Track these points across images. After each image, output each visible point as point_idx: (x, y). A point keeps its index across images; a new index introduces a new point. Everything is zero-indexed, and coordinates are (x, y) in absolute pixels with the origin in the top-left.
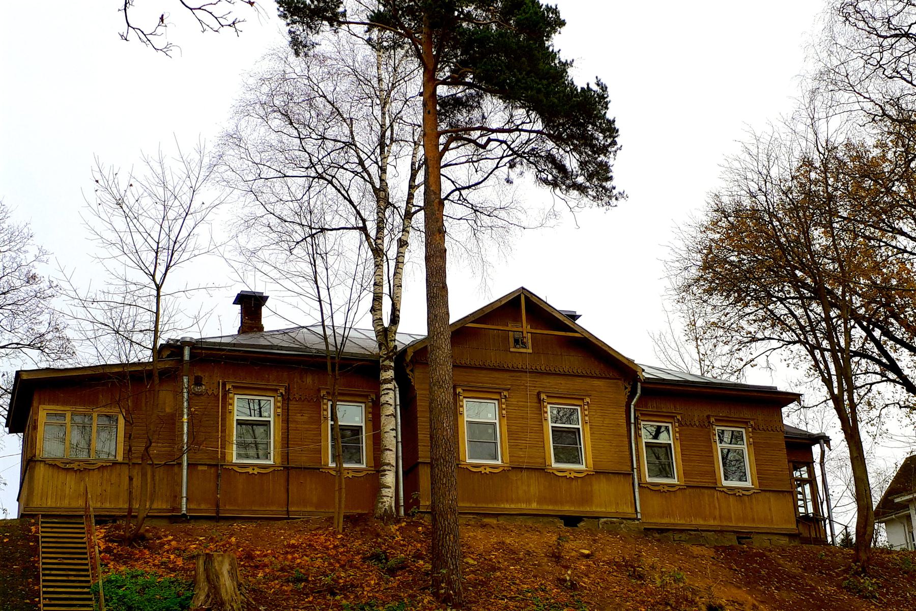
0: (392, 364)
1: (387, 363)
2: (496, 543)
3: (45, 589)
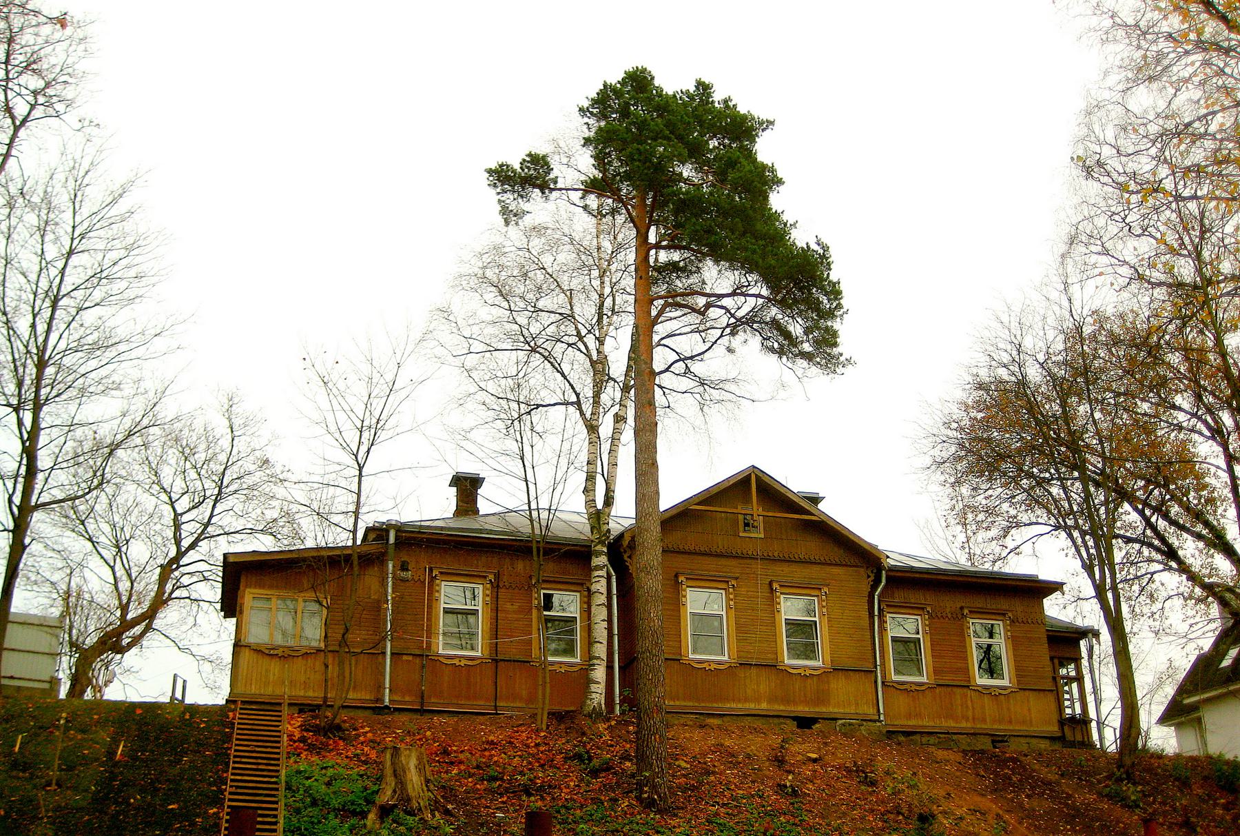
0: (605, 550)
1: (599, 548)
2: (713, 745)
3: (232, 777)
